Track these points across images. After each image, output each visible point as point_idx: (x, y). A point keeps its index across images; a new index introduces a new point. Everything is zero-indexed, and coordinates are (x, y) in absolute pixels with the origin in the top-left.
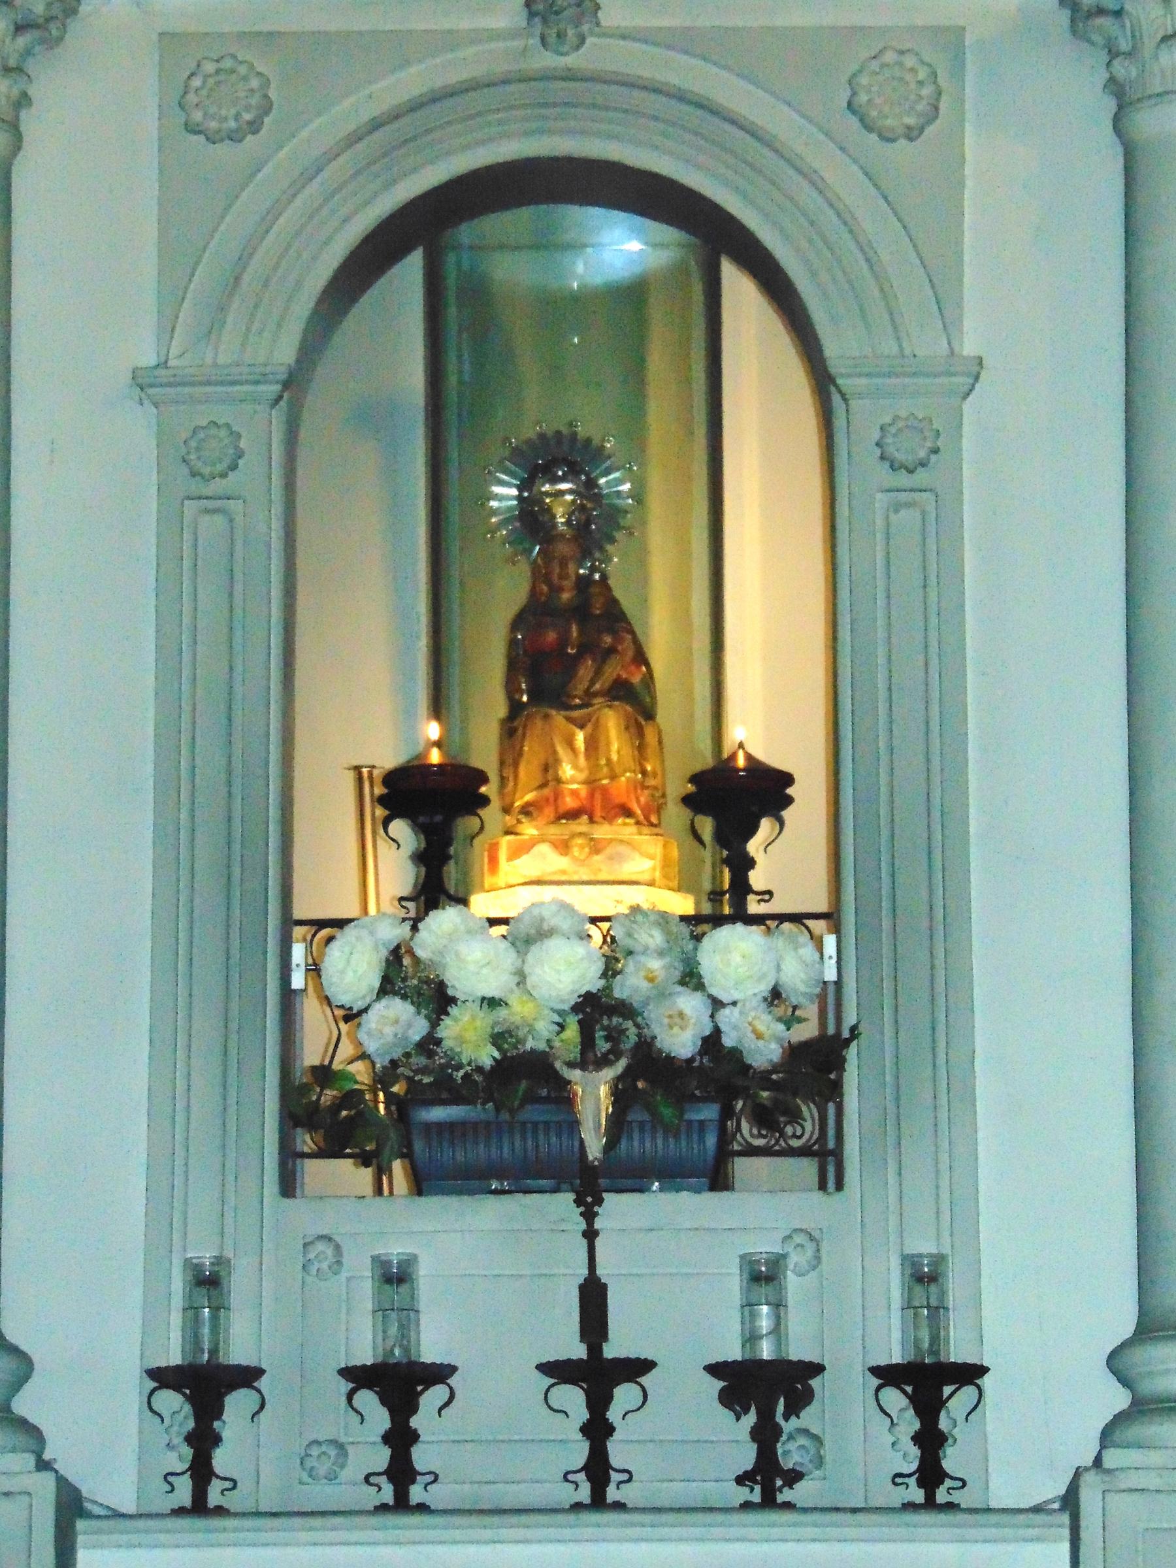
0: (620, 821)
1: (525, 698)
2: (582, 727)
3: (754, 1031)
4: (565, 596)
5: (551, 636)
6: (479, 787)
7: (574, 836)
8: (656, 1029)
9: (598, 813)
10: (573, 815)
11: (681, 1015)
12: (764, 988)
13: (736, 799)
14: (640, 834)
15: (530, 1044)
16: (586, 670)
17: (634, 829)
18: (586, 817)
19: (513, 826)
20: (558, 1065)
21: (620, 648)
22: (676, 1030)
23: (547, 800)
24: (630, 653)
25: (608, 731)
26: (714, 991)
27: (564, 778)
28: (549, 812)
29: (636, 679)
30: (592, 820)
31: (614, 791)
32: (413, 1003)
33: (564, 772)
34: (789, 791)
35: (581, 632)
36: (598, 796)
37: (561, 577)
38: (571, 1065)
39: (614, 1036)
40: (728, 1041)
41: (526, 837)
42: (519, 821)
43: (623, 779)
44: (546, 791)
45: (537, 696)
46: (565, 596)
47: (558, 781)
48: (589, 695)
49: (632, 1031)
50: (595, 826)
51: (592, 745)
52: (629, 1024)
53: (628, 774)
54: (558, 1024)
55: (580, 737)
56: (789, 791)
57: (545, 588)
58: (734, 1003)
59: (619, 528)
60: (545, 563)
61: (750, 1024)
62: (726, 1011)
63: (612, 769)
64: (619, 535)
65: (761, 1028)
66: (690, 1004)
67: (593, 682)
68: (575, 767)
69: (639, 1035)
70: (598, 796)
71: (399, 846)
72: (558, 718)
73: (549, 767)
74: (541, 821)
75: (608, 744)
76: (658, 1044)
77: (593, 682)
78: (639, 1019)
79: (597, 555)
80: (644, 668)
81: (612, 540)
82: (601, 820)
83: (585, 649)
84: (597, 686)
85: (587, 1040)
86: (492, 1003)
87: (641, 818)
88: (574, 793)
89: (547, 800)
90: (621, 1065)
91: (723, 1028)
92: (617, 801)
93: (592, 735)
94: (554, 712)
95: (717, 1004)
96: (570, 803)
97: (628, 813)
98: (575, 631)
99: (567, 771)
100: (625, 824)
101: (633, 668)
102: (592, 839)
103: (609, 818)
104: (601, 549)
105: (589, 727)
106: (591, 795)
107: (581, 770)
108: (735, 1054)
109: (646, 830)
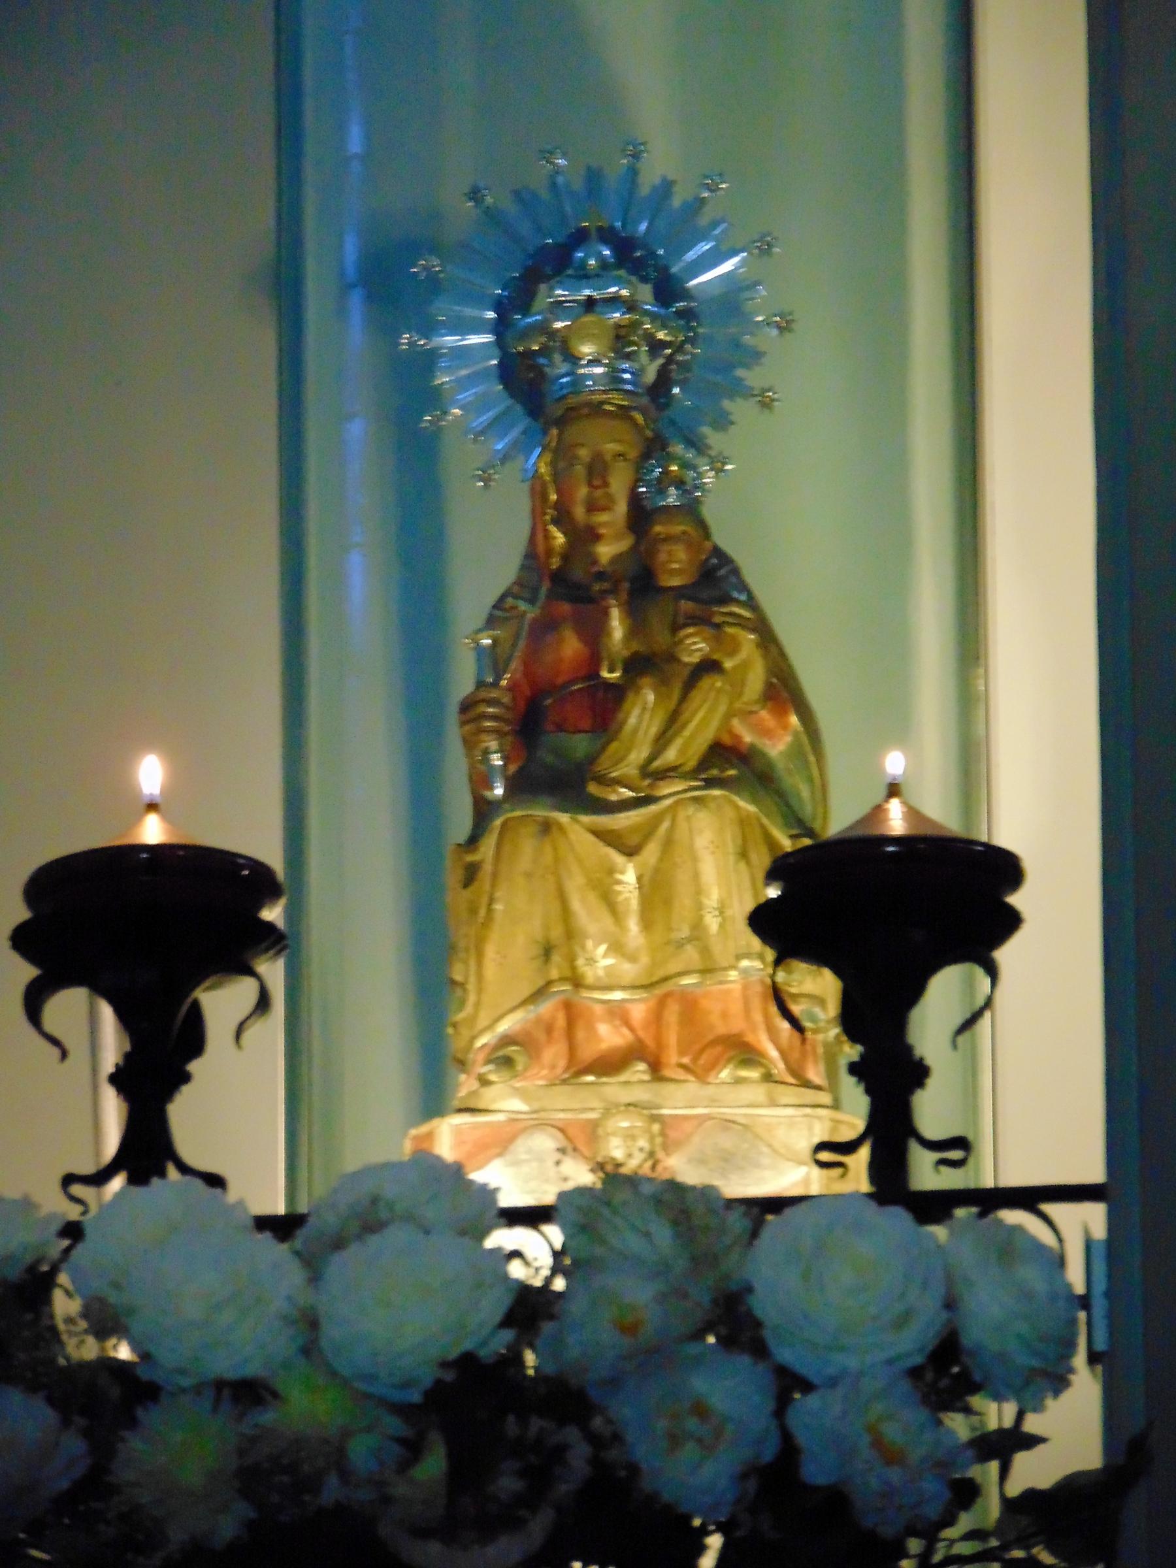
0: (725, 1074)
1: (499, 791)
2: (631, 852)
3: (878, 1443)
4: (606, 551)
5: (571, 646)
6: (259, 907)
7: (611, 1109)
8: (644, 1449)
9: (672, 1056)
10: (609, 1065)
11: (700, 1410)
12: (913, 1342)
13: (887, 917)
14: (773, 1103)
15: (332, 1491)
16: (643, 713)
17: (758, 1092)
18: (642, 1066)
19: (473, 1094)
20: (385, 1530)
21: (728, 664)
22: (689, 1451)
23: (549, 1029)
24: (756, 680)
25: (695, 859)
26: (785, 1355)
27: (590, 978)
28: (554, 1054)
29: (776, 748)
30: (656, 1069)
31: (712, 1008)
32: (50, 1401)
33: (591, 961)
34: (1015, 900)
35: (636, 629)
36: (672, 1014)
37: (592, 507)
38: (422, 1533)
39: (542, 1466)
40: (817, 1470)
41: (500, 1117)
42: (484, 1082)
43: (733, 975)
44: (546, 1008)
45: (524, 785)
46: (606, 551)
47: (577, 982)
48: (654, 774)
49: (579, 1455)
50: (669, 1088)
51: (657, 894)
52: (572, 1434)
53: (745, 963)
54: (402, 1441)
55: (629, 875)
56: (1015, 900)
57: (559, 538)
58: (833, 1382)
59: (738, 390)
60: (556, 475)
61: (871, 1429)
62: (813, 1401)
63: (705, 951)
64: (737, 408)
65: (892, 1432)
66: (729, 1389)
67: (662, 741)
68: (617, 948)
69: (596, 1462)
70: (672, 1014)
71: (64, 1055)
72: (576, 828)
73: (557, 948)
74: (537, 1079)
75: (699, 891)
76: (647, 1484)
77: (662, 741)
78: (597, 1422)
79: (678, 449)
80: (794, 720)
81: (722, 422)
82: (680, 1074)
83: (639, 666)
84: (671, 755)
85: (465, 1474)
86: (248, 1393)
87: (779, 1068)
88: (618, 1013)
89: (549, 1029)
90: (539, 1526)
91: (802, 1438)
92: (721, 1029)
93: (657, 870)
94: (564, 818)
95: (789, 1384)
96: (609, 1036)
97: (747, 1055)
98: (617, 627)
99: (600, 961)
100: (739, 1081)
101: (765, 716)
102: (654, 1118)
103: (701, 1072)
104: (695, 443)
105: (651, 852)
106: (657, 1017)
107: (632, 959)
108: (836, 1501)
109: (791, 1095)
